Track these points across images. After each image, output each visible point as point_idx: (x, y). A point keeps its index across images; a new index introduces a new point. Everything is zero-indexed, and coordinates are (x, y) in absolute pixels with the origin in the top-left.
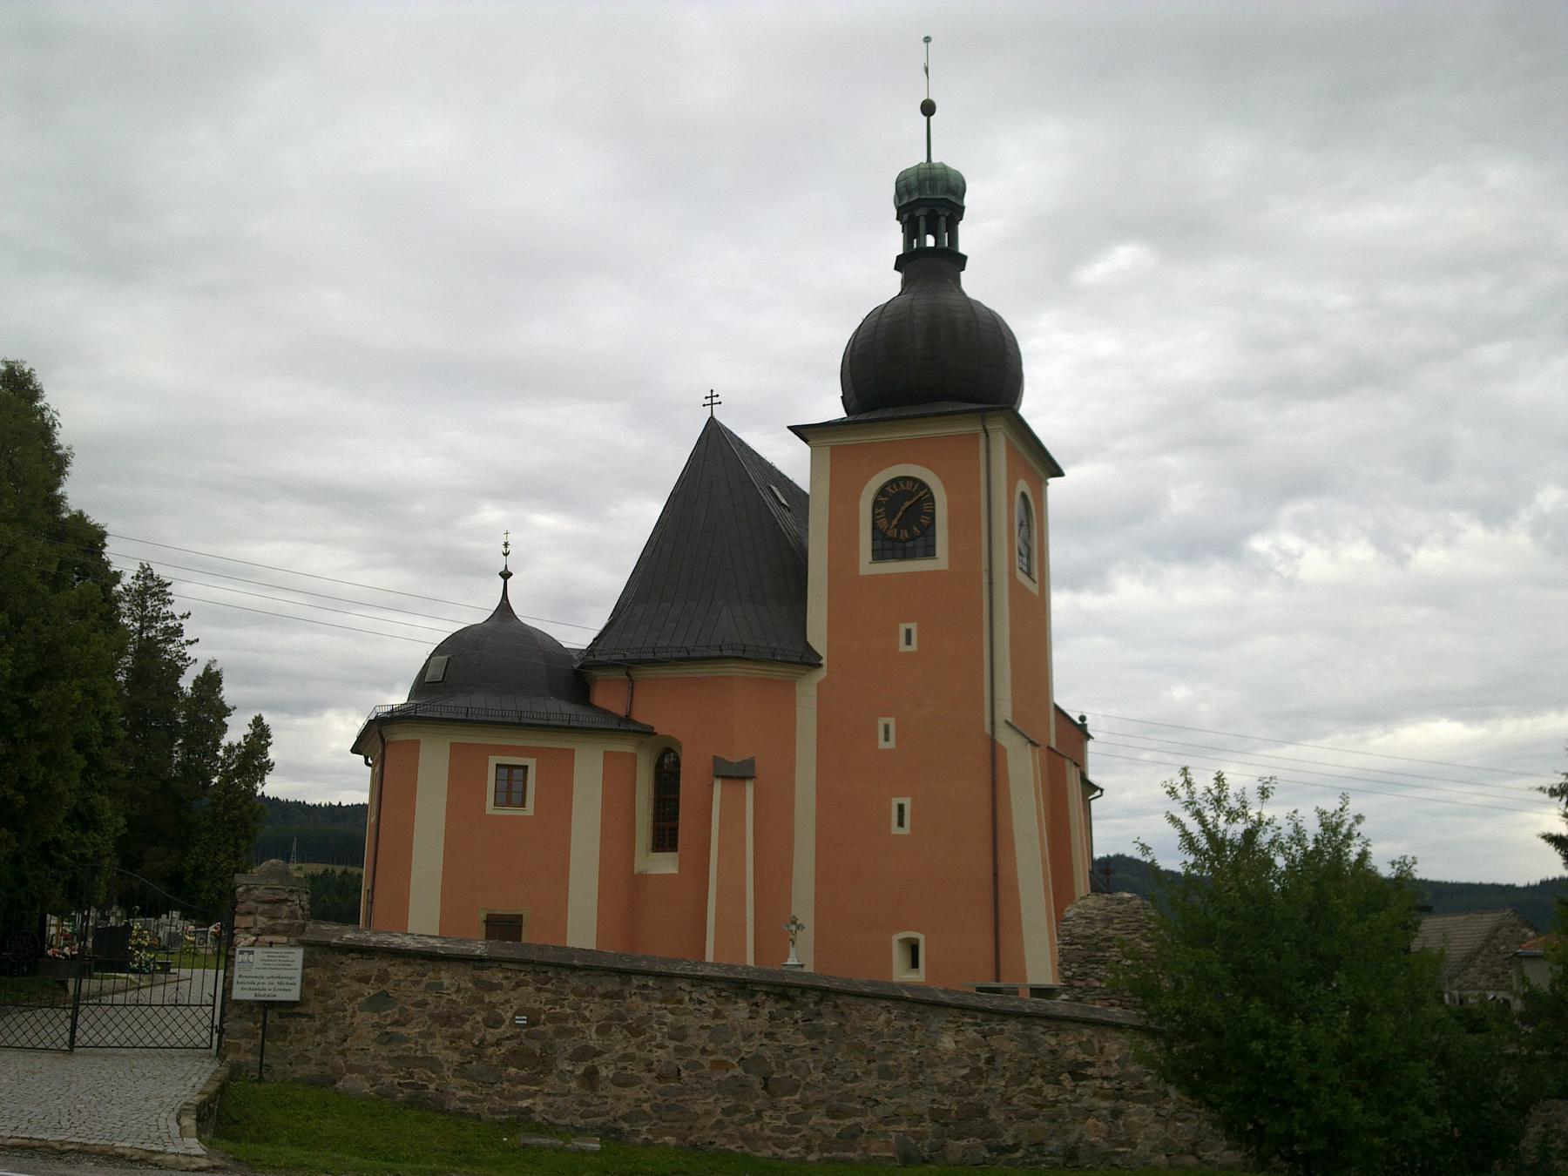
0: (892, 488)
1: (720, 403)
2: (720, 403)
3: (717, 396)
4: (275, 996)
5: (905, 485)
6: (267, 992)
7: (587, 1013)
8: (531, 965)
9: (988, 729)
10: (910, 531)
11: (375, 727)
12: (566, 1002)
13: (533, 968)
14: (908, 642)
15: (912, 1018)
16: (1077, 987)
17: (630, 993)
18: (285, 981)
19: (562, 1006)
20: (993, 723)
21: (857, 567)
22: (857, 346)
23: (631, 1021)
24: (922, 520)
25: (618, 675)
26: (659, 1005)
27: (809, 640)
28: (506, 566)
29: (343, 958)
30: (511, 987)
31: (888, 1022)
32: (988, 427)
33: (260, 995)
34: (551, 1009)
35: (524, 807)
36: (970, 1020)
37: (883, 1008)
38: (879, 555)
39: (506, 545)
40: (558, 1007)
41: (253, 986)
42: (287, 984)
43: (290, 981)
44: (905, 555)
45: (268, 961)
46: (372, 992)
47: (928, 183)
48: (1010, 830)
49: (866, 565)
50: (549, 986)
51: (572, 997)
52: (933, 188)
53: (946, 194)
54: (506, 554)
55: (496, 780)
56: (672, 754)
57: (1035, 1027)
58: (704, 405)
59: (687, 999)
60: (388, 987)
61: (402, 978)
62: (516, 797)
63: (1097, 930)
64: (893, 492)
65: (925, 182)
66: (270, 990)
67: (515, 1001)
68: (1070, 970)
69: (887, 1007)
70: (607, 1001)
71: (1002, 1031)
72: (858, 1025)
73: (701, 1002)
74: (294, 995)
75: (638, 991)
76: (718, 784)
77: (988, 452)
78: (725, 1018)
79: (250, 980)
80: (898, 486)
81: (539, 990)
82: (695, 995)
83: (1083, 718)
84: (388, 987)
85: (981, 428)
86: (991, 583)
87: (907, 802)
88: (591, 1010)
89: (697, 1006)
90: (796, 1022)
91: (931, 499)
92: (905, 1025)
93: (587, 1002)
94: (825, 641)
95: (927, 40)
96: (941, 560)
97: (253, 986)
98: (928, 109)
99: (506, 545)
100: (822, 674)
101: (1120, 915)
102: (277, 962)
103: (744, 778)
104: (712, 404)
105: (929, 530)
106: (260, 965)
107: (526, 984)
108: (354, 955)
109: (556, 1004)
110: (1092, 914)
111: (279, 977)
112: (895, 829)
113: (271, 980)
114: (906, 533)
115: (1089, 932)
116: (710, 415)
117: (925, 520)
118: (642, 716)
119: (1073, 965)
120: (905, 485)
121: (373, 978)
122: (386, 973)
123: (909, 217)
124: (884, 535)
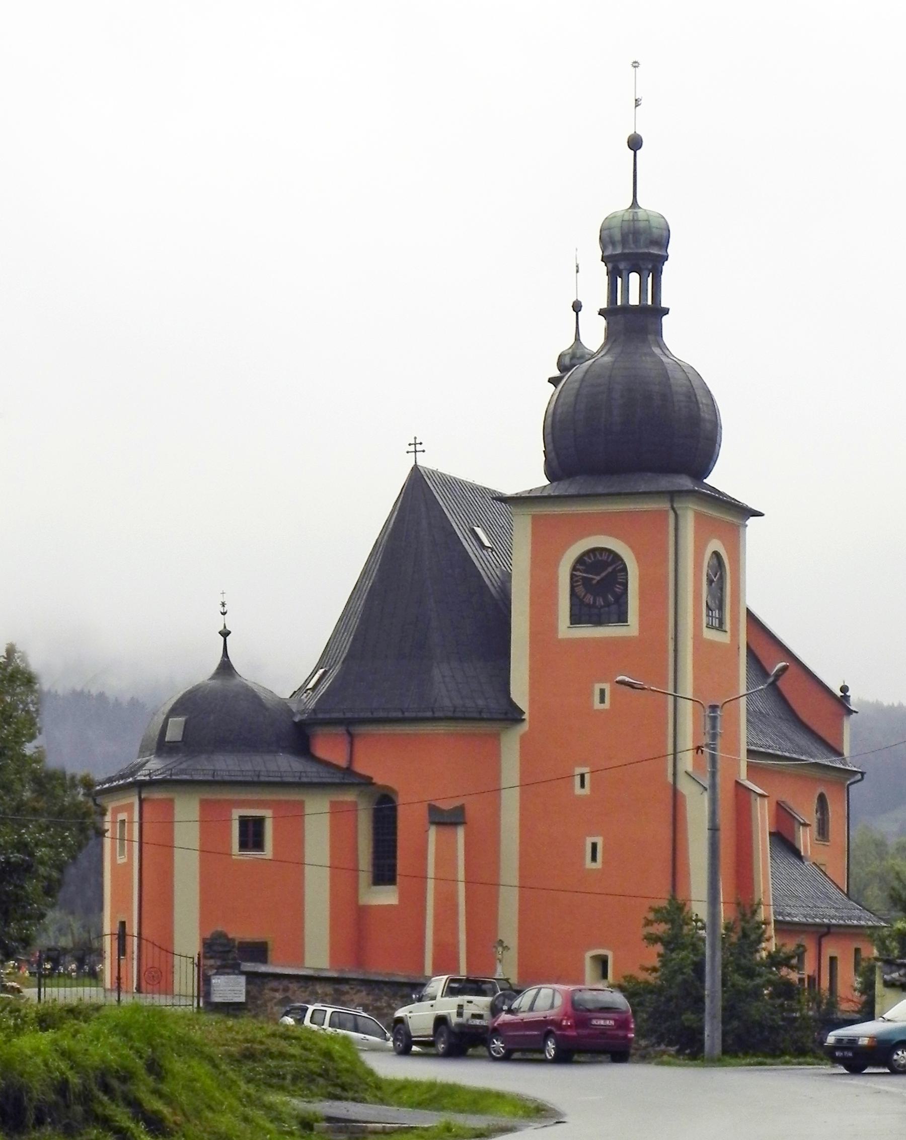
0: (590, 558)
2: (424, 451)
3: (421, 444)
5: (601, 556)
14: (602, 700)
19: (381, 1002)
20: (675, 774)
22: (559, 411)
24: (617, 590)
25: (341, 730)
27: (512, 696)
28: (225, 624)
32: (675, 506)
38: (576, 619)
39: (223, 605)
44: (598, 621)
46: (281, 997)
47: (631, 236)
48: (687, 865)
49: (565, 629)
52: (636, 241)
53: (647, 247)
54: (224, 614)
58: (408, 452)
60: (289, 994)
64: (590, 561)
65: (628, 236)
74: (242, 998)
76: (432, 832)
77: (676, 529)
80: (595, 556)
83: (844, 689)
84: (289, 994)
85: (670, 506)
86: (676, 650)
87: (599, 841)
91: (624, 569)
95: (635, 64)
96: (632, 628)
98: (635, 143)
99: (223, 605)
100: (524, 727)
103: (455, 824)
104: (416, 451)
105: (621, 600)
106: (224, 984)
107: (362, 991)
112: (589, 864)
116: (414, 463)
117: (618, 589)
118: (361, 767)
120: (601, 556)
122: (288, 987)
124: (581, 601)
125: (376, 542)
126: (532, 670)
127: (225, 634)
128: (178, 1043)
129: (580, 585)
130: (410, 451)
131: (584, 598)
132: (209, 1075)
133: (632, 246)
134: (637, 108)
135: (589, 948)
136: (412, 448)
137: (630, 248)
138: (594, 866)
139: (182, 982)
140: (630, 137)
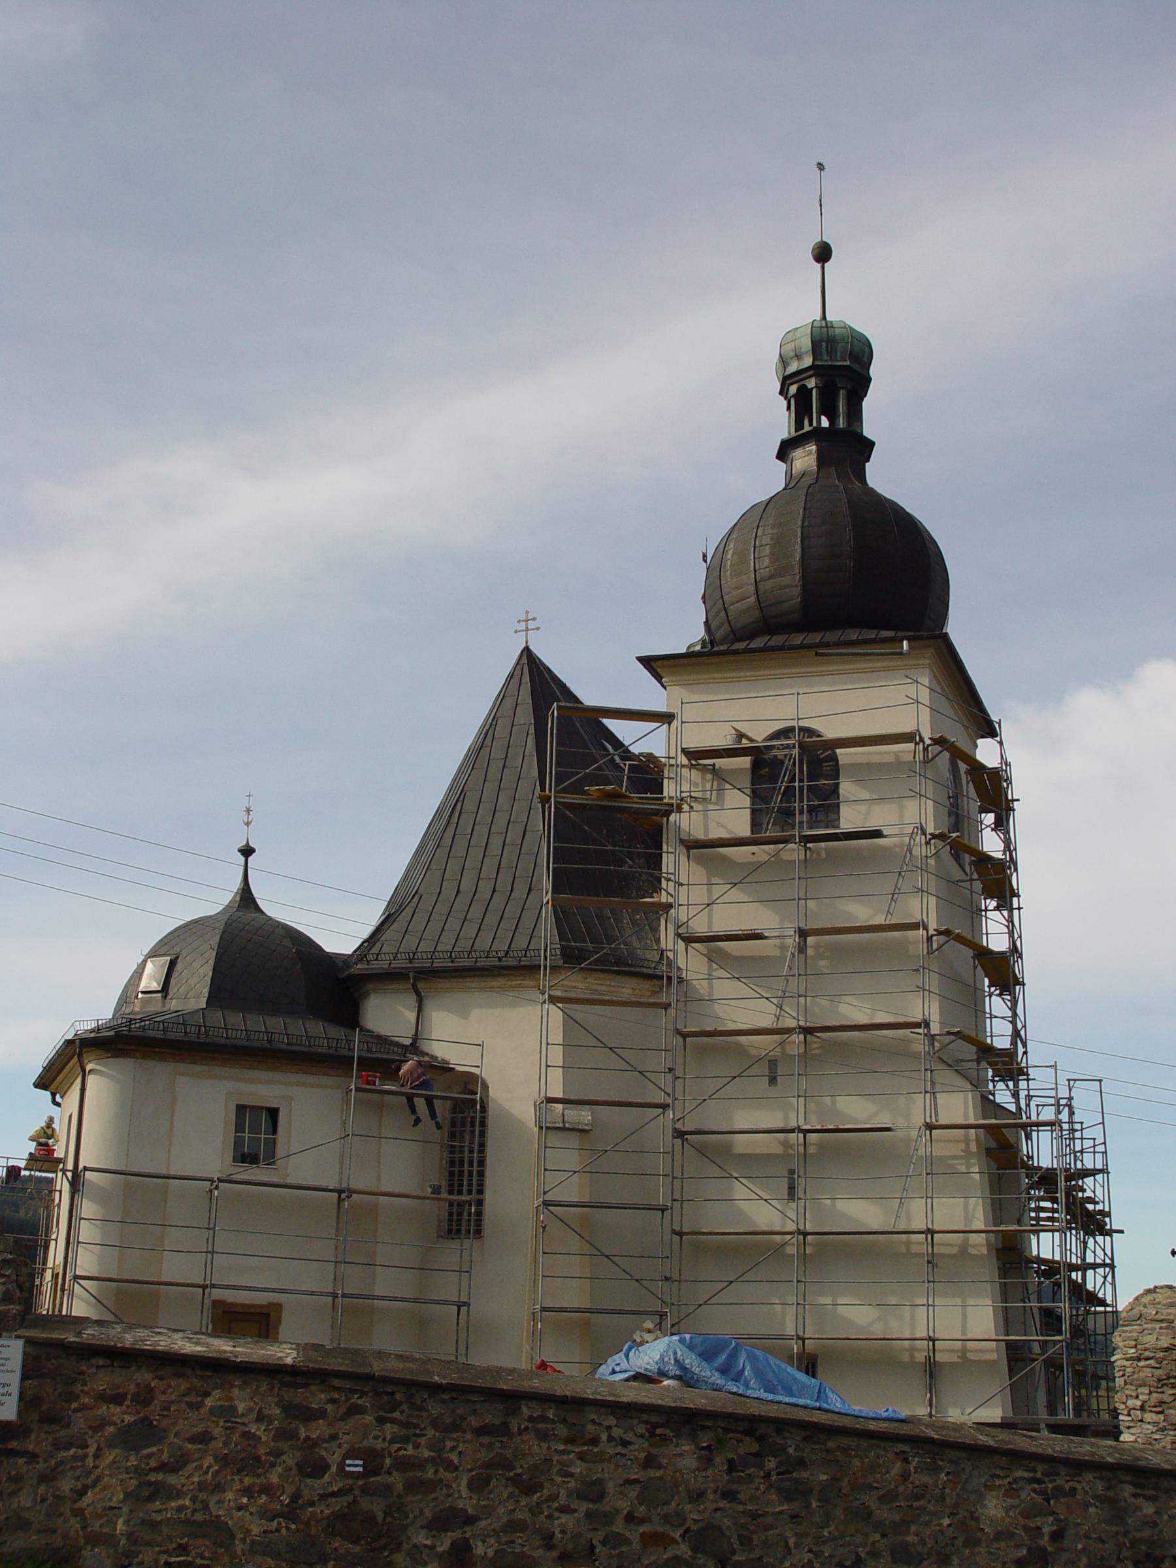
1: (538, 629)
3: (534, 619)
7: (454, 1457)
12: (422, 1440)
19: (417, 1446)
23: (519, 1471)
26: (561, 1447)
31: (905, 1476)
34: (400, 1449)
36: (1026, 1475)
39: (248, 811)
40: (410, 1447)
46: (128, 1418)
47: (824, 344)
50: (396, 1415)
51: (430, 1432)
52: (831, 352)
54: (248, 824)
58: (516, 632)
59: (604, 1437)
61: (173, 1397)
68: (1137, 1397)
69: (904, 1452)
70: (485, 1440)
73: (625, 1443)
81: (381, 1421)
82: (617, 1432)
89: (619, 1449)
90: (768, 1475)
93: (455, 1440)
95: (821, 167)
99: (248, 811)
104: (527, 630)
108: (101, 1362)
109: (407, 1443)
110: (1170, 1314)
121: (129, 1397)
123: (798, 389)
125: (469, 749)
127: (247, 852)
130: (518, 629)
132: (337, 1478)
133: (826, 358)
134: (524, 645)
136: (523, 626)
137: (821, 360)
140: (715, 569)
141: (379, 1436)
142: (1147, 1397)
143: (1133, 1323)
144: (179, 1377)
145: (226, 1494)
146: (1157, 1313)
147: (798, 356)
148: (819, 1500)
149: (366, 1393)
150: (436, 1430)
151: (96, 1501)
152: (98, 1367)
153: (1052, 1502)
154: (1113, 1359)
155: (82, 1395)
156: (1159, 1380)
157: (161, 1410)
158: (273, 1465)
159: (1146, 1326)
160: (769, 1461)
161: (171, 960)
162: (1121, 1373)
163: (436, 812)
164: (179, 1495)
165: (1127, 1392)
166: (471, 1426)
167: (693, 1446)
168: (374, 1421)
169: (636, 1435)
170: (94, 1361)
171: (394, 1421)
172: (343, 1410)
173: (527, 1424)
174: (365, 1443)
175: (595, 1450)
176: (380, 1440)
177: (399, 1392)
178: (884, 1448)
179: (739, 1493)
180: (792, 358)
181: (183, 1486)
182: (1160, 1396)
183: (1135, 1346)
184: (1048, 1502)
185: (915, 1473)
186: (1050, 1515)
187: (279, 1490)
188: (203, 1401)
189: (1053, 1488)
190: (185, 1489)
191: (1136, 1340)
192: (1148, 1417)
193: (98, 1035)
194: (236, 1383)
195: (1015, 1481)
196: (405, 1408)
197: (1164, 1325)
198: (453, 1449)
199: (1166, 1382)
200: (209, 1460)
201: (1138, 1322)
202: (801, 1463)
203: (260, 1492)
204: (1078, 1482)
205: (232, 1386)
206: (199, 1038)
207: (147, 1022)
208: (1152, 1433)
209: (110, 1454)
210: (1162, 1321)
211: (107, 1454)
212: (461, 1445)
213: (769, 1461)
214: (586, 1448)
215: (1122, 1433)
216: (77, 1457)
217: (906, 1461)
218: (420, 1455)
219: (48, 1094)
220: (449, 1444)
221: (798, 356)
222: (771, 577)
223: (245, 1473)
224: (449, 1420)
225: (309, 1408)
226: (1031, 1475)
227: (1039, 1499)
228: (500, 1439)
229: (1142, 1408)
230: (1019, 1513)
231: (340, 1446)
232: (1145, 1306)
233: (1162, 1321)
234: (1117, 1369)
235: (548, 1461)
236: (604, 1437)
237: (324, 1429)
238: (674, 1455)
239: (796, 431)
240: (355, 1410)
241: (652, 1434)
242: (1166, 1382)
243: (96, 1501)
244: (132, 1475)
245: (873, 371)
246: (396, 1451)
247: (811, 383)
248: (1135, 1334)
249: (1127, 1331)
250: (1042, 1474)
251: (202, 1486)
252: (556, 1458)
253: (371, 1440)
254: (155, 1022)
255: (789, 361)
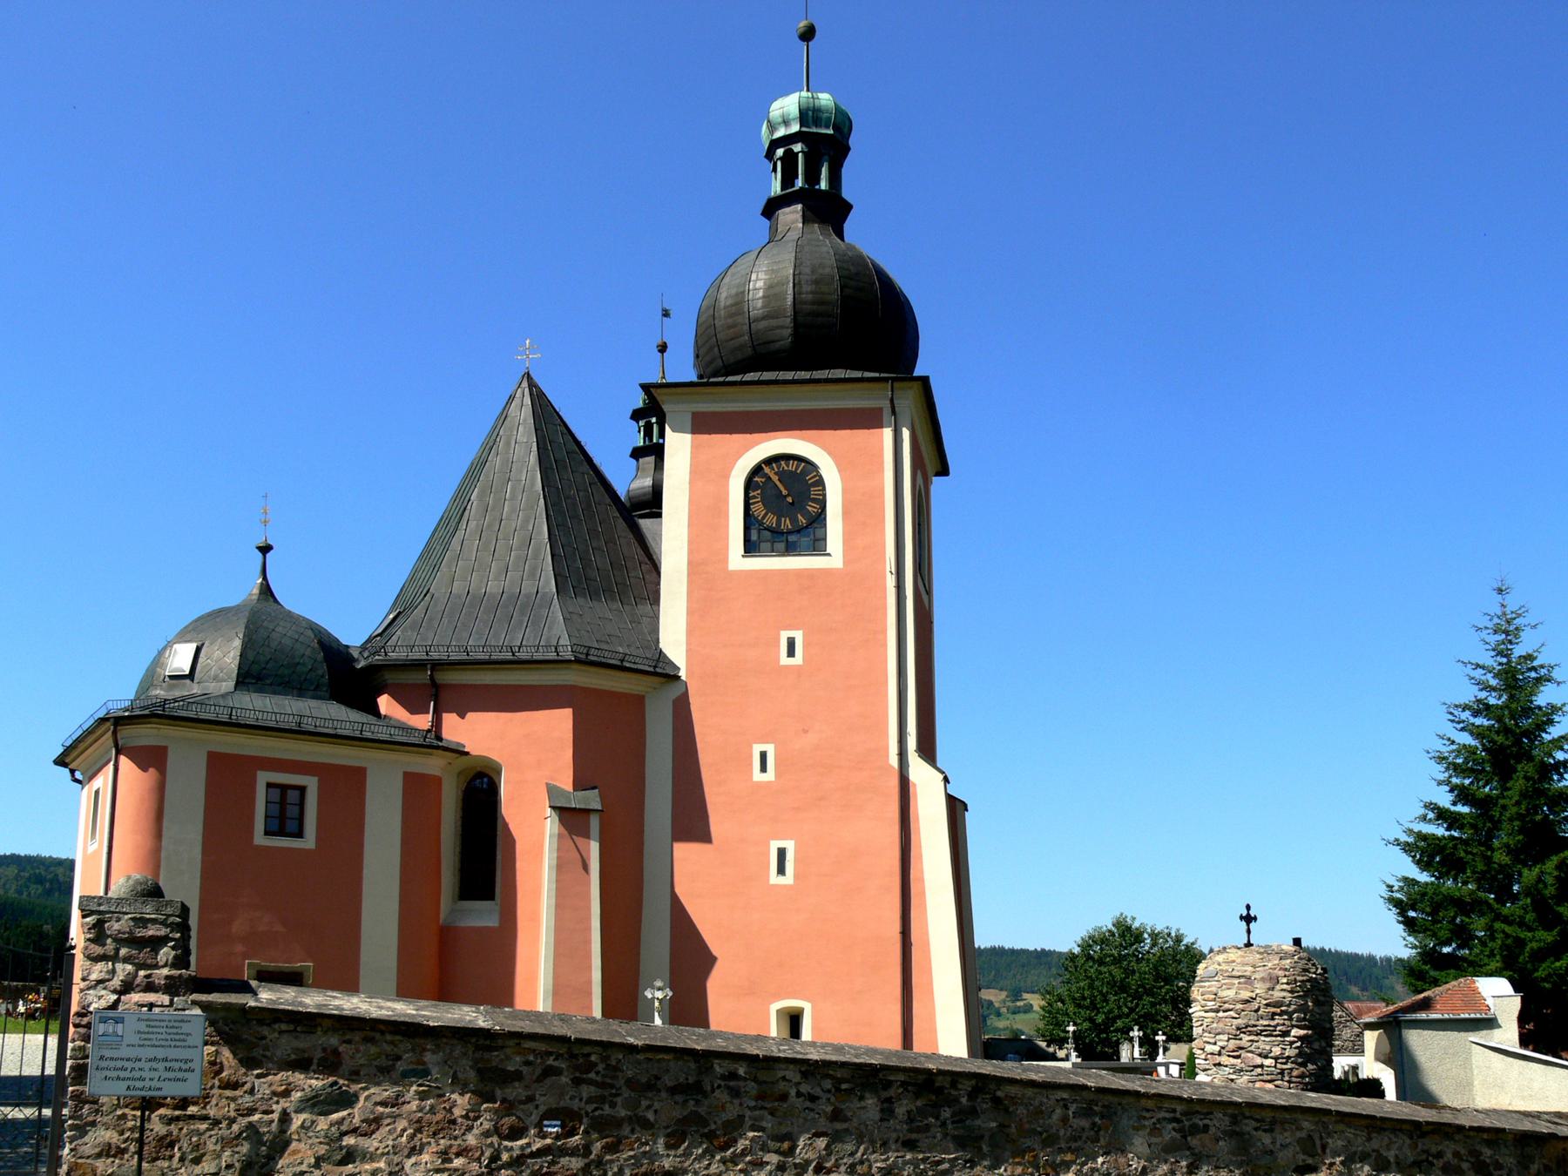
4: (160, 1089)
6: (147, 1084)
7: (650, 1116)
8: (566, 1045)
9: (894, 761)
10: (794, 520)
11: (109, 725)
12: (619, 1100)
13: (569, 1049)
15: (1096, 1114)
16: (1226, 1066)
17: (713, 1086)
18: (176, 1065)
19: (613, 1105)
21: (725, 560)
23: (713, 1127)
24: (810, 508)
26: (753, 1103)
29: (265, 1031)
30: (534, 1077)
31: (1065, 1120)
33: (135, 1089)
34: (596, 1109)
35: (302, 837)
36: (1167, 1115)
37: (1057, 1100)
40: (607, 1107)
41: (122, 1074)
42: (180, 1070)
43: (184, 1067)
44: (790, 550)
45: (148, 1033)
47: (810, 113)
50: (592, 1075)
51: (626, 1093)
55: (267, 802)
56: (485, 780)
57: (1247, 1121)
59: (793, 1092)
61: (362, 1061)
62: (291, 826)
63: (1258, 991)
64: (786, 468)
65: (807, 114)
66: (151, 1079)
67: (543, 1099)
68: (1215, 1044)
69: (1063, 1099)
70: (679, 1098)
71: (1206, 1128)
72: (1027, 1126)
73: (813, 1098)
75: (723, 1083)
78: (846, 1120)
79: (119, 1064)
81: (577, 1082)
82: (805, 1088)
85: (886, 404)
87: (790, 846)
88: (656, 1111)
89: (808, 1104)
90: (944, 1124)
91: (820, 482)
92: (1085, 1123)
93: (651, 1099)
94: (684, 648)
97: (122, 1074)
101: (1287, 973)
102: (162, 1037)
105: (819, 519)
106: (135, 1039)
107: (555, 1072)
108: (284, 1027)
109: (603, 1103)
110: (1246, 971)
111: (166, 1060)
112: (774, 879)
113: (154, 1065)
114: (788, 521)
115: (1245, 995)
117: (812, 508)
119: (1221, 1037)
121: (315, 1061)
125: (472, 464)
126: (690, 612)
127: (265, 549)
128: (1553, 744)
129: (758, 502)
131: (764, 517)
135: (778, 997)
138: (781, 880)
139: (49, 1047)
141: (575, 1097)
142: (1226, 1043)
143: (1211, 979)
144: (368, 1041)
145: (422, 1156)
146: (1233, 970)
147: (786, 123)
148: (990, 1146)
149: (562, 1055)
150: (632, 1090)
151: (285, 1166)
152: (281, 1032)
153: (1189, 1138)
154: (1190, 1011)
155: (264, 1059)
156: (1238, 1029)
157: (350, 1075)
158: (470, 1129)
159: (1223, 982)
160: (945, 1111)
161: (197, 647)
162: (1200, 1023)
163: (441, 519)
164: (373, 1158)
165: (1205, 1039)
166: (666, 1085)
167: (876, 1100)
168: (570, 1082)
169: (823, 1090)
170: (276, 1026)
171: (591, 1082)
172: (538, 1071)
173: (719, 1082)
174: (562, 1104)
175: (785, 1106)
176: (577, 1100)
177: (595, 1053)
178: (1047, 1097)
179: (918, 1141)
180: (780, 124)
181: (377, 1149)
182: (1238, 1042)
183: (1214, 1000)
184: (1186, 1139)
185: (1074, 1117)
186: (1188, 1150)
187: (477, 1151)
188: (394, 1065)
189: (1191, 1126)
190: (379, 1152)
191: (1216, 995)
192: (1224, 1060)
193: (133, 714)
194: (428, 1047)
195: (1158, 1120)
196: (600, 1069)
197: (1242, 980)
198: (649, 1107)
199: (1244, 1030)
200: (401, 1124)
201: (1216, 978)
202: (973, 1112)
203: (458, 1155)
204: (1211, 1120)
205: (424, 1050)
206: (230, 718)
207: (181, 703)
208: (1229, 1073)
209: (297, 1119)
210: (1239, 977)
211: (295, 1120)
212: (656, 1103)
213: (945, 1111)
214: (776, 1104)
215: (1197, 1074)
216: (176, 1121)
217: (1066, 1107)
218: (616, 1114)
219: (66, 771)
220: (644, 1103)
221: (786, 123)
222: (764, 318)
223: (441, 1136)
224: (644, 1080)
225: (504, 1070)
226: (1172, 1115)
227: (1178, 1136)
228: (694, 1097)
229: (1220, 1054)
230: (1162, 1150)
231: (537, 1107)
232: (1219, 964)
233: (1239, 977)
234: (1194, 1020)
235: (741, 1117)
236: (793, 1092)
237: (520, 1090)
238: (858, 1108)
239: (782, 190)
240: (549, 1072)
241: (838, 1090)
242: (1244, 1030)
243: (285, 1166)
244: (322, 1140)
245: (852, 142)
246: (593, 1111)
247: (797, 148)
248: (1214, 989)
249: (1205, 987)
250: (1181, 1114)
251: (396, 1150)
252: (748, 1113)
253: (568, 1101)
254: (189, 703)
255: (777, 126)
